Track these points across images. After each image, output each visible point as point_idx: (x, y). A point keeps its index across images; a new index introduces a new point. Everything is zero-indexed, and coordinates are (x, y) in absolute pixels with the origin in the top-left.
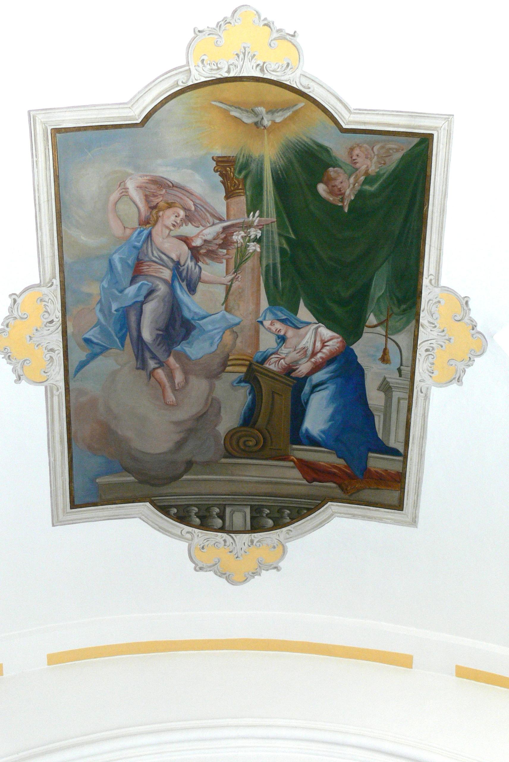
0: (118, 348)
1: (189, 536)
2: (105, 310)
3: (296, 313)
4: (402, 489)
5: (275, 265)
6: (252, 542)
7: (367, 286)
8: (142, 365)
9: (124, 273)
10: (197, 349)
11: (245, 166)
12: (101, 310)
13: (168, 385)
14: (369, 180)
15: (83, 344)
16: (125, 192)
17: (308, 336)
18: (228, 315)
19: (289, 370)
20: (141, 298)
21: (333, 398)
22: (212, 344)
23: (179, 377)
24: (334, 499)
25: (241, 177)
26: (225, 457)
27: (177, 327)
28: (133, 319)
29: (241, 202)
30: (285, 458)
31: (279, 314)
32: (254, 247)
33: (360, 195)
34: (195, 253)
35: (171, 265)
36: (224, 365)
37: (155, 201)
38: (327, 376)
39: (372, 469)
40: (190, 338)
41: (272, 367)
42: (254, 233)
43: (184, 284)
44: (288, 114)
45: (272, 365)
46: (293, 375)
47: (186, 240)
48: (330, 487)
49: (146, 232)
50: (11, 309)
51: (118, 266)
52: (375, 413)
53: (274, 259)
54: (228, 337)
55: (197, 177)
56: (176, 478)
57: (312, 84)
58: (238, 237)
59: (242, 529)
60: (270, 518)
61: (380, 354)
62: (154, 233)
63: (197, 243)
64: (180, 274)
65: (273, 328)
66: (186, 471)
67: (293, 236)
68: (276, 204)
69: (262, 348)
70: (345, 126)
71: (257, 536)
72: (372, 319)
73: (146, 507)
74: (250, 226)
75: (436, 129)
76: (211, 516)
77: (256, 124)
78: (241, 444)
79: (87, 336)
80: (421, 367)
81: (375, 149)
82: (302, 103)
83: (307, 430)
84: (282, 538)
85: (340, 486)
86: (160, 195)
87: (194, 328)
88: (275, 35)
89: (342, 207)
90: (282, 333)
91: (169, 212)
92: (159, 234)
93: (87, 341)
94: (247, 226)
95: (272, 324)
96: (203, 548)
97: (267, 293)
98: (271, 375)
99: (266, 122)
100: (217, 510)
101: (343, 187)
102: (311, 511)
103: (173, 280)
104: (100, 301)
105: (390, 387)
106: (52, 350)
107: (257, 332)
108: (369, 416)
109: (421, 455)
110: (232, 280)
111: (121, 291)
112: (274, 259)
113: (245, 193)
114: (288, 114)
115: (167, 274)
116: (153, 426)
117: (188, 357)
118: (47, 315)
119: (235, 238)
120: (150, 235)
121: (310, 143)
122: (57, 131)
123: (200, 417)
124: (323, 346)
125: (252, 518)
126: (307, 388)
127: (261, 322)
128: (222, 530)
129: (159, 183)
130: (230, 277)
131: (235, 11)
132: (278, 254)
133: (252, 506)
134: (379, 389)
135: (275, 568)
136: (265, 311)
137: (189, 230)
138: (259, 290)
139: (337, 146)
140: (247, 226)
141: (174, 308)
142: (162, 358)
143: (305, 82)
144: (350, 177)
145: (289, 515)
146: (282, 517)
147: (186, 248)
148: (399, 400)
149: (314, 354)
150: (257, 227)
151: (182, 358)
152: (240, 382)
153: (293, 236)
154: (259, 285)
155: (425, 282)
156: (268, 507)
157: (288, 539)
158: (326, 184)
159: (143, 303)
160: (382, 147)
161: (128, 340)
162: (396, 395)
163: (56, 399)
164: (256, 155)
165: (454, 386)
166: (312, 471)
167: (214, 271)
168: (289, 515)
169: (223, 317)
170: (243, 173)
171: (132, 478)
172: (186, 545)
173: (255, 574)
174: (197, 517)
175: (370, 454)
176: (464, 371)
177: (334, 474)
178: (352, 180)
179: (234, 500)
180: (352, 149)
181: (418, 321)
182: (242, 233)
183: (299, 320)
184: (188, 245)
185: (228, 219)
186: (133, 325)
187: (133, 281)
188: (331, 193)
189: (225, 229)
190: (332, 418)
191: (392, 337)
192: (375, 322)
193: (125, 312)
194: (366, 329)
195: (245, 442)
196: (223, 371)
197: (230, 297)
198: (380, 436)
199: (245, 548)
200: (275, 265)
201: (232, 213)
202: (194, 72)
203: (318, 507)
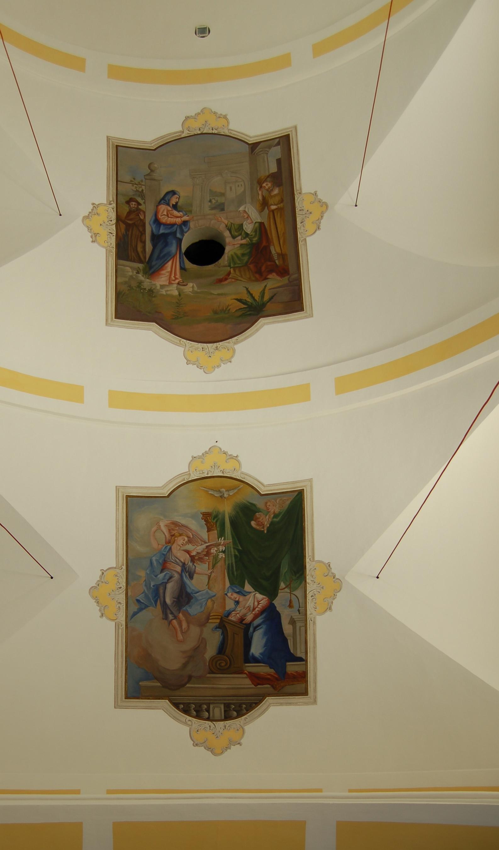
0: (153, 607)
1: (189, 723)
2: (147, 585)
3: (244, 587)
4: (306, 682)
5: (232, 563)
6: (225, 726)
7: (279, 567)
8: (166, 618)
9: (158, 568)
10: (194, 610)
11: (216, 516)
12: (146, 585)
13: (179, 629)
14: (276, 516)
15: (136, 602)
16: (159, 528)
17: (251, 598)
18: (210, 592)
19: (242, 620)
20: (166, 581)
21: (265, 633)
22: (201, 607)
23: (184, 625)
24: (270, 695)
25: (215, 521)
26: (209, 673)
27: (184, 597)
28: (161, 591)
29: (215, 533)
30: (242, 672)
31: (235, 589)
32: (222, 555)
33: (272, 524)
34: (193, 559)
35: (181, 564)
36: (208, 619)
37: (174, 532)
38: (262, 620)
39: (289, 672)
40: (190, 604)
41: (233, 619)
42: (222, 548)
43: (187, 574)
44: (236, 491)
45: (233, 618)
46: (244, 622)
47: (188, 552)
48: (267, 688)
49: (169, 547)
50: (101, 577)
51: (155, 563)
52: (288, 638)
53: (232, 561)
54: (210, 603)
55: (194, 522)
56: (183, 685)
57: (246, 477)
58: (213, 551)
59: (219, 719)
60: (235, 711)
61: (288, 604)
62: (172, 547)
63: (194, 553)
64: (185, 569)
65: (233, 597)
66: (188, 682)
67: (240, 548)
68: (232, 535)
69: (227, 609)
70: (262, 493)
71: (228, 723)
72: (282, 585)
73: (165, 703)
74: (219, 545)
75: (304, 486)
76: (202, 710)
77: (221, 496)
78: (218, 665)
79: (138, 598)
80: (310, 606)
81: (277, 501)
82: (242, 485)
83: (252, 654)
84: (242, 724)
85: (273, 686)
86: (176, 530)
87: (192, 598)
88: (228, 457)
89: (263, 531)
90: (237, 599)
91: (180, 538)
92: (175, 548)
93: (138, 601)
94: (218, 545)
95: (232, 595)
96: (198, 731)
97: (229, 578)
98: (232, 623)
99: (226, 495)
100: (205, 706)
101: (263, 522)
102: (257, 704)
103: (182, 572)
104: (145, 580)
105: (295, 621)
106: (120, 603)
107: (224, 600)
108: (285, 640)
109: (315, 658)
110: (211, 573)
111: (156, 576)
112: (232, 561)
113: (217, 529)
114: (236, 491)
115: (179, 569)
116: (171, 654)
117: (189, 614)
118: (118, 584)
119: (212, 551)
120: (170, 548)
121: (246, 503)
122: (127, 497)
123: (196, 649)
124: (259, 604)
125: (225, 711)
126: (251, 629)
127: (226, 594)
128: (208, 719)
129: (175, 524)
130: (210, 571)
131: (210, 449)
132: (233, 558)
133: (224, 704)
134: (289, 623)
135: (239, 743)
136: (228, 588)
137: (189, 547)
138: (224, 577)
139: (260, 503)
140: (218, 545)
141: (182, 587)
142: (176, 613)
143: (243, 476)
144: (266, 516)
145: (245, 708)
146: (242, 710)
147: (188, 556)
148: (300, 627)
149: (254, 609)
150: (223, 545)
151: (187, 614)
152: (216, 628)
153: (240, 548)
154: (225, 574)
155: (307, 560)
156: (234, 704)
157: (245, 724)
158: (255, 521)
159: (166, 583)
160: (281, 500)
161: (158, 603)
162: (298, 625)
163: (120, 631)
164: (221, 510)
165: (328, 613)
166: (256, 679)
167: (201, 568)
168: (245, 708)
169: (207, 593)
170: (215, 520)
171: (159, 684)
172: (187, 729)
173: (228, 748)
174: (195, 711)
175: (288, 663)
176: (332, 603)
177: (269, 679)
178: (267, 517)
179: (215, 700)
180: (266, 503)
181: (306, 581)
182: (216, 549)
183: (245, 591)
184: (189, 554)
185: (209, 542)
186: (162, 595)
187: (162, 571)
188: (258, 525)
189: (207, 547)
190: (266, 645)
191: (293, 593)
192: (284, 587)
193: (157, 588)
194: (280, 591)
195: (220, 664)
196: (207, 622)
197: (210, 582)
198: (292, 651)
199: (221, 731)
200: (232, 563)
201: (211, 538)
202: (192, 474)
203: (261, 701)
